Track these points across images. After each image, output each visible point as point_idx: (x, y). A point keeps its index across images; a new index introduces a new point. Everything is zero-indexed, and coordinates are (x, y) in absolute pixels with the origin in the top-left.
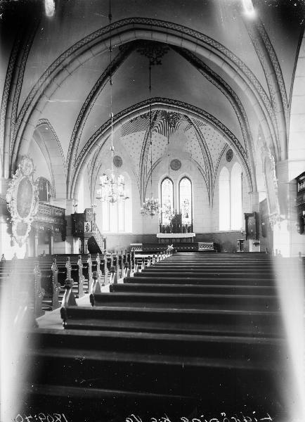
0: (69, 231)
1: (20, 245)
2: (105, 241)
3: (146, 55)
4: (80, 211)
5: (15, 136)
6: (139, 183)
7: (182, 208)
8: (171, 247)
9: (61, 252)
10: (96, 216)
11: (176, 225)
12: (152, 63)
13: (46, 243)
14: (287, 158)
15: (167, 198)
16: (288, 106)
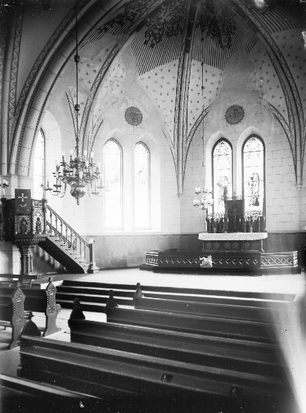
6: (175, 151)
8: (208, 261)
11: (235, 217)
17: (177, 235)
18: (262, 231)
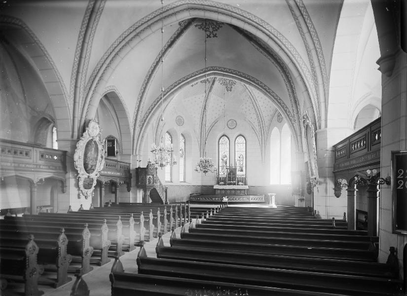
0: (133, 182)
1: (86, 197)
3: (203, 29)
4: (143, 165)
5: (83, 102)
9: (126, 201)
10: (157, 170)
12: (209, 36)
13: (113, 193)
14: (326, 126)
17: (199, 186)
18: (245, 184)
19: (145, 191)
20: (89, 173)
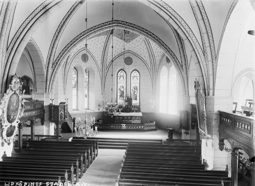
1: (9, 144)
2: (74, 121)
4: (56, 103)
7: (132, 92)
14: (214, 95)
15: (122, 85)
16: (216, 57)
19: (57, 124)
20: (11, 123)
